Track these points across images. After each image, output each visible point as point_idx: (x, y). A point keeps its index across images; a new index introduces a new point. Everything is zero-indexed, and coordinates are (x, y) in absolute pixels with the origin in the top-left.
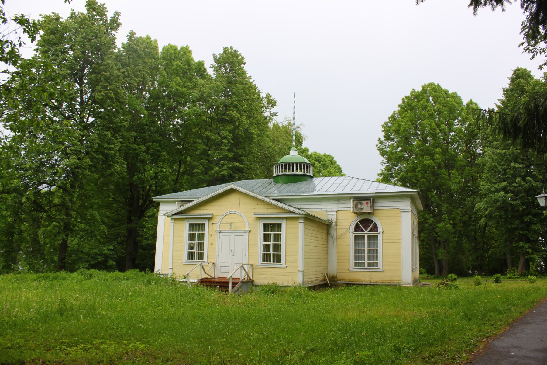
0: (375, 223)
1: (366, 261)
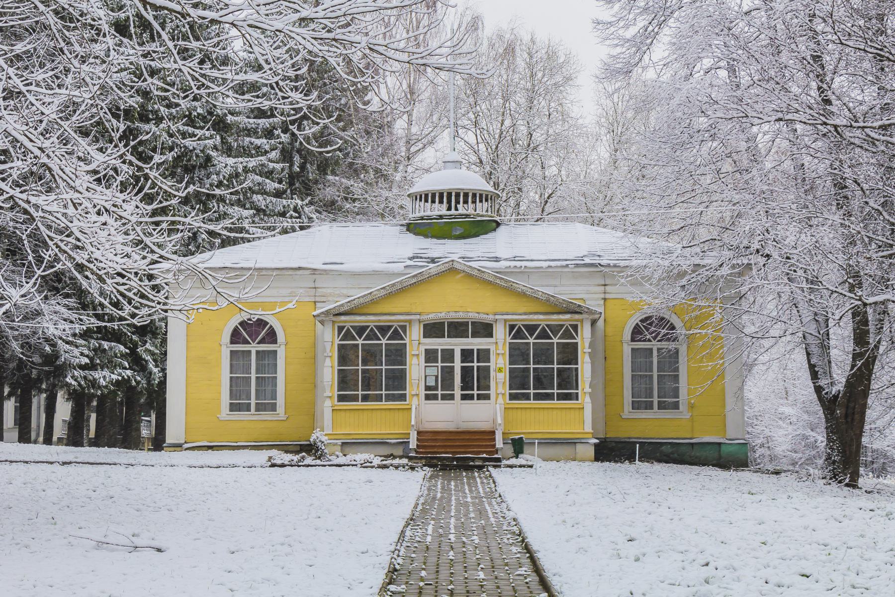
0: (271, 326)
1: (253, 402)
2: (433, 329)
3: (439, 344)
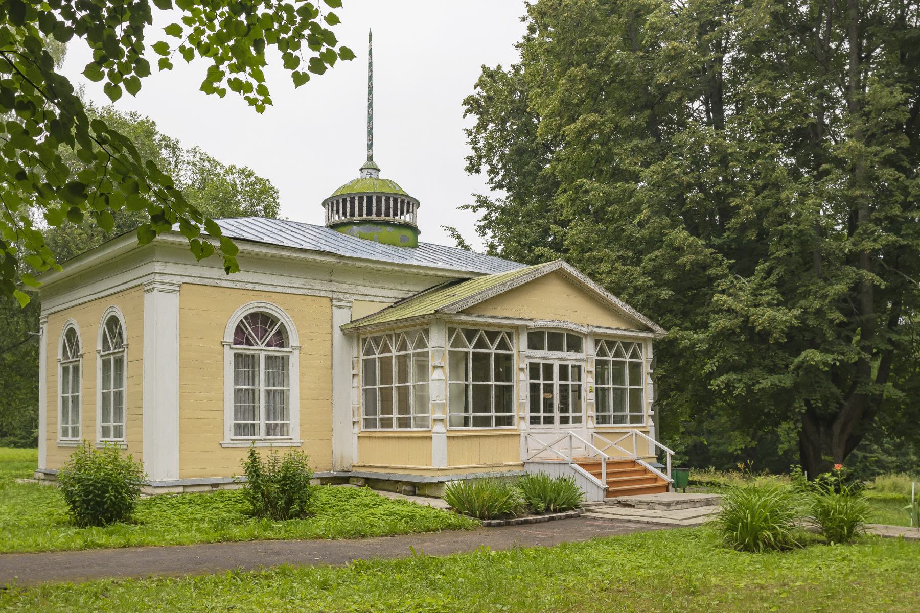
2: (536, 340)
3: (544, 356)
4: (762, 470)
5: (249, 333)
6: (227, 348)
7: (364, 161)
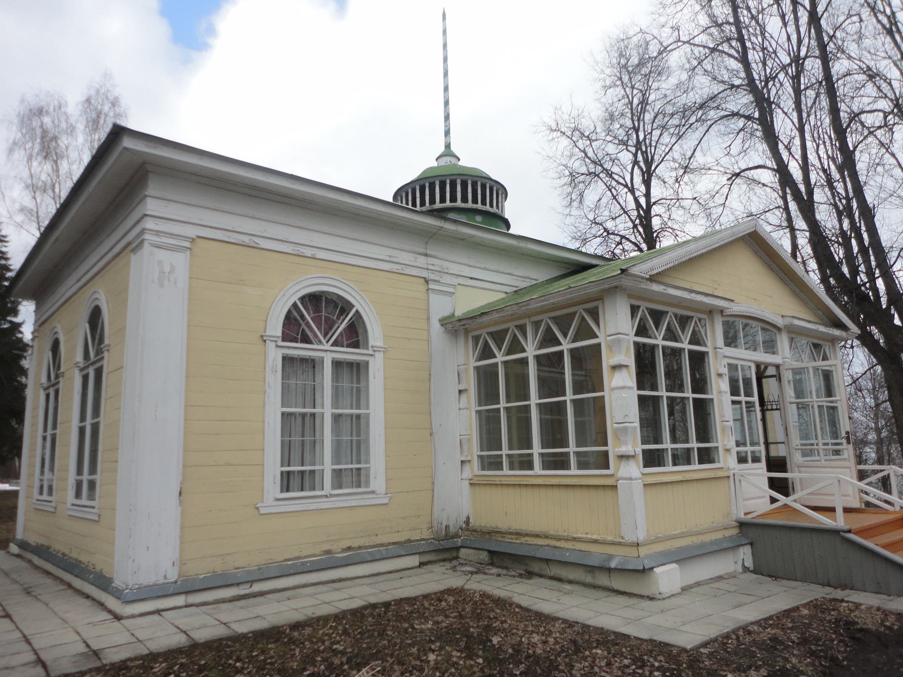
4: (14, 431)
5: (308, 325)
6: (271, 346)
7: (441, 149)
